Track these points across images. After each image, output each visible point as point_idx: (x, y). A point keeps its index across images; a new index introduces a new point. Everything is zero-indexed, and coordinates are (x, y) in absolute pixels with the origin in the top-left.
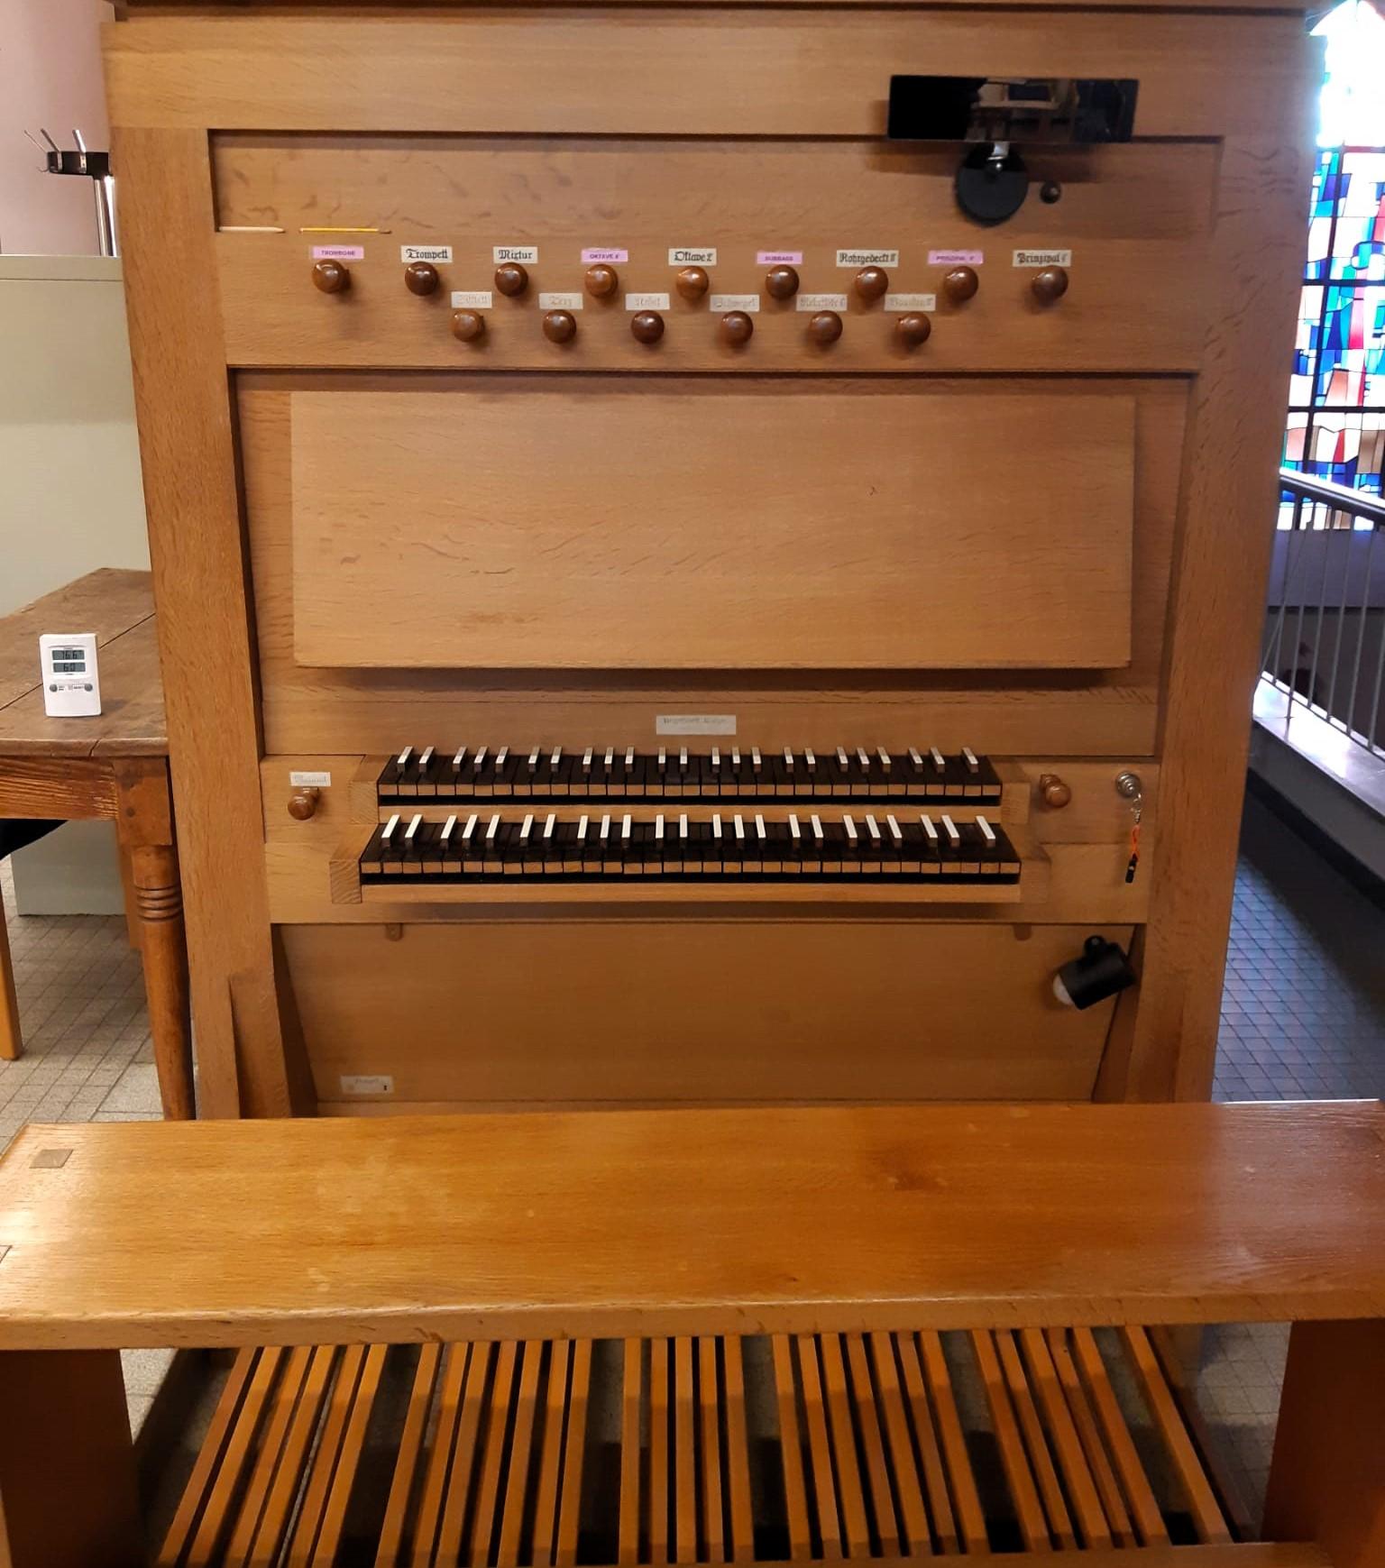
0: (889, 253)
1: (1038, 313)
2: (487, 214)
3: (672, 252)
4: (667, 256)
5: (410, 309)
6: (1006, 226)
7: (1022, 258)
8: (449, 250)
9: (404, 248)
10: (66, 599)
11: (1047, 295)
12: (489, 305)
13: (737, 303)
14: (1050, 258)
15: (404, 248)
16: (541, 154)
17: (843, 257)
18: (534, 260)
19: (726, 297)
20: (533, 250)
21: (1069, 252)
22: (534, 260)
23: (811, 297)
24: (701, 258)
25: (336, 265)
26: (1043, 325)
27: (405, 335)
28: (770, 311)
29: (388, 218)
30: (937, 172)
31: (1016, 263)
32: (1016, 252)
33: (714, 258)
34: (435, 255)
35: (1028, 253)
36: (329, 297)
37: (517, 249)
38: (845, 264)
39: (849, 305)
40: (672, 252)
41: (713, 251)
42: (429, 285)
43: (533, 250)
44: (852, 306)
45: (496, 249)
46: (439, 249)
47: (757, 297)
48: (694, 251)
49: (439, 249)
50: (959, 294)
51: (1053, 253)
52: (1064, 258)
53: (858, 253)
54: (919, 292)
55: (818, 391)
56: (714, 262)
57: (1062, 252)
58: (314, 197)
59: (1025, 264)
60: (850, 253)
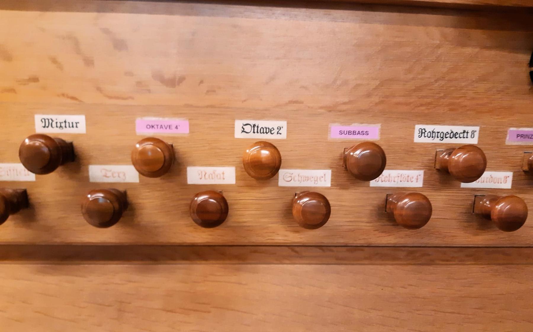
0: (470, 129)
2: (35, 79)
4: (289, 131)
7: (48, 124)
8: (283, 124)
13: (307, 179)
15: (477, 129)
16: (94, 14)
17: (422, 132)
18: (82, 129)
19: (296, 172)
20: (81, 119)
22: (82, 129)
24: (270, 131)
28: (343, 187)
30: (514, 49)
33: (284, 131)
36: (157, 180)
37: (61, 118)
38: (424, 140)
39: (425, 181)
40: (238, 124)
41: (283, 124)
43: (81, 119)
44: (336, 183)
48: (262, 124)
51: (458, 129)
54: (408, 168)
56: (284, 134)
60: (429, 128)
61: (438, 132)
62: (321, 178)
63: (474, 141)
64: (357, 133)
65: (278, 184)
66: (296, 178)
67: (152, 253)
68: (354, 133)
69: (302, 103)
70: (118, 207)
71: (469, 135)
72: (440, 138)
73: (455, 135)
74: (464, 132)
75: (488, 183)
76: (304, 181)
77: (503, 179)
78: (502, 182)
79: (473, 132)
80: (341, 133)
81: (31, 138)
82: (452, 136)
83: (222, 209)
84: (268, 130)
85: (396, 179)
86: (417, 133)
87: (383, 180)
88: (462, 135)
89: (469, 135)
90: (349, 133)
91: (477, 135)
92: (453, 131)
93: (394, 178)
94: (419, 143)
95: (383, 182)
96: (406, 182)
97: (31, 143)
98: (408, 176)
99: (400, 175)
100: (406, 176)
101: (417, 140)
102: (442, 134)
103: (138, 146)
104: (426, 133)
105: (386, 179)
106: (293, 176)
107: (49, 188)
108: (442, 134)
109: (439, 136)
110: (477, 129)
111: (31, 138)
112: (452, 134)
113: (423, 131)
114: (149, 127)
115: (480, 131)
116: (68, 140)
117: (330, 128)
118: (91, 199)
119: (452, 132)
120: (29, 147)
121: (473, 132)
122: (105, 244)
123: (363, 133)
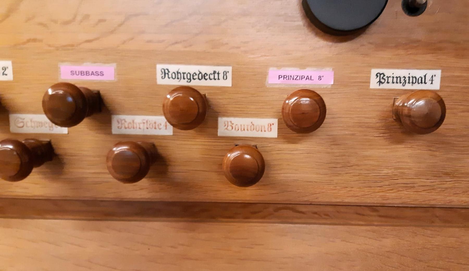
0: (221, 69)
1: (399, 142)
6: (362, 40)
7: (381, 78)
11: (415, 124)
12: (274, 133)
13: (253, 127)
14: (415, 80)
15: (229, 69)
17: (165, 73)
21: (438, 73)
23: (128, 118)
26: (408, 156)
31: (374, 84)
32: (374, 71)
33: (10, 72)
35: (388, 72)
47: (275, 121)
50: (306, 119)
51: (419, 73)
52: (433, 79)
53: (183, 68)
55: (327, 202)
57: (430, 73)
59: (385, 86)
60: (173, 68)
61: (184, 73)
62: (265, 127)
63: (436, 86)
64: (90, 73)
65: (217, 135)
66: (29, 124)
67: (194, 211)
68: (87, 73)
69: (41, 41)
70: (146, 160)
71: (221, 76)
72: (186, 80)
73: (204, 76)
74: (215, 72)
75: (267, 132)
76: (37, 127)
77: (266, 127)
78: (266, 130)
79: (225, 73)
80: (73, 73)
81: (55, 87)
82: (200, 77)
83: (175, 162)
84: (414, 79)
85: (142, 126)
86: (159, 75)
87: (127, 126)
88: (212, 77)
89: (221, 76)
90: (82, 73)
91: (229, 75)
92: (201, 71)
93: (139, 124)
94: (163, 85)
95: (128, 129)
96: (153, 129)
97: (54, 93)
98: (155, 123)
99: (145, 121)
100: (153, 122)
101: (160, 81)
102: (189, 75)
103: (168, 96)
104: (170, 74)
105: (130, 126)
106: (25, 121)
107: (80, 140)
108: (189, 75)
109: (185, 77)
110: (229, 69)
111: (55, 87)
112: (200, 75)
113: (167, 72)
114: (171, 75)
115: (233, 71)
116: (94, 88)
117: (60, 68)
118: (116, 152)
119: (200, 73)
120: (52, 96)
121: (225, 73)
122: (131, 200)
123: (97, 74)
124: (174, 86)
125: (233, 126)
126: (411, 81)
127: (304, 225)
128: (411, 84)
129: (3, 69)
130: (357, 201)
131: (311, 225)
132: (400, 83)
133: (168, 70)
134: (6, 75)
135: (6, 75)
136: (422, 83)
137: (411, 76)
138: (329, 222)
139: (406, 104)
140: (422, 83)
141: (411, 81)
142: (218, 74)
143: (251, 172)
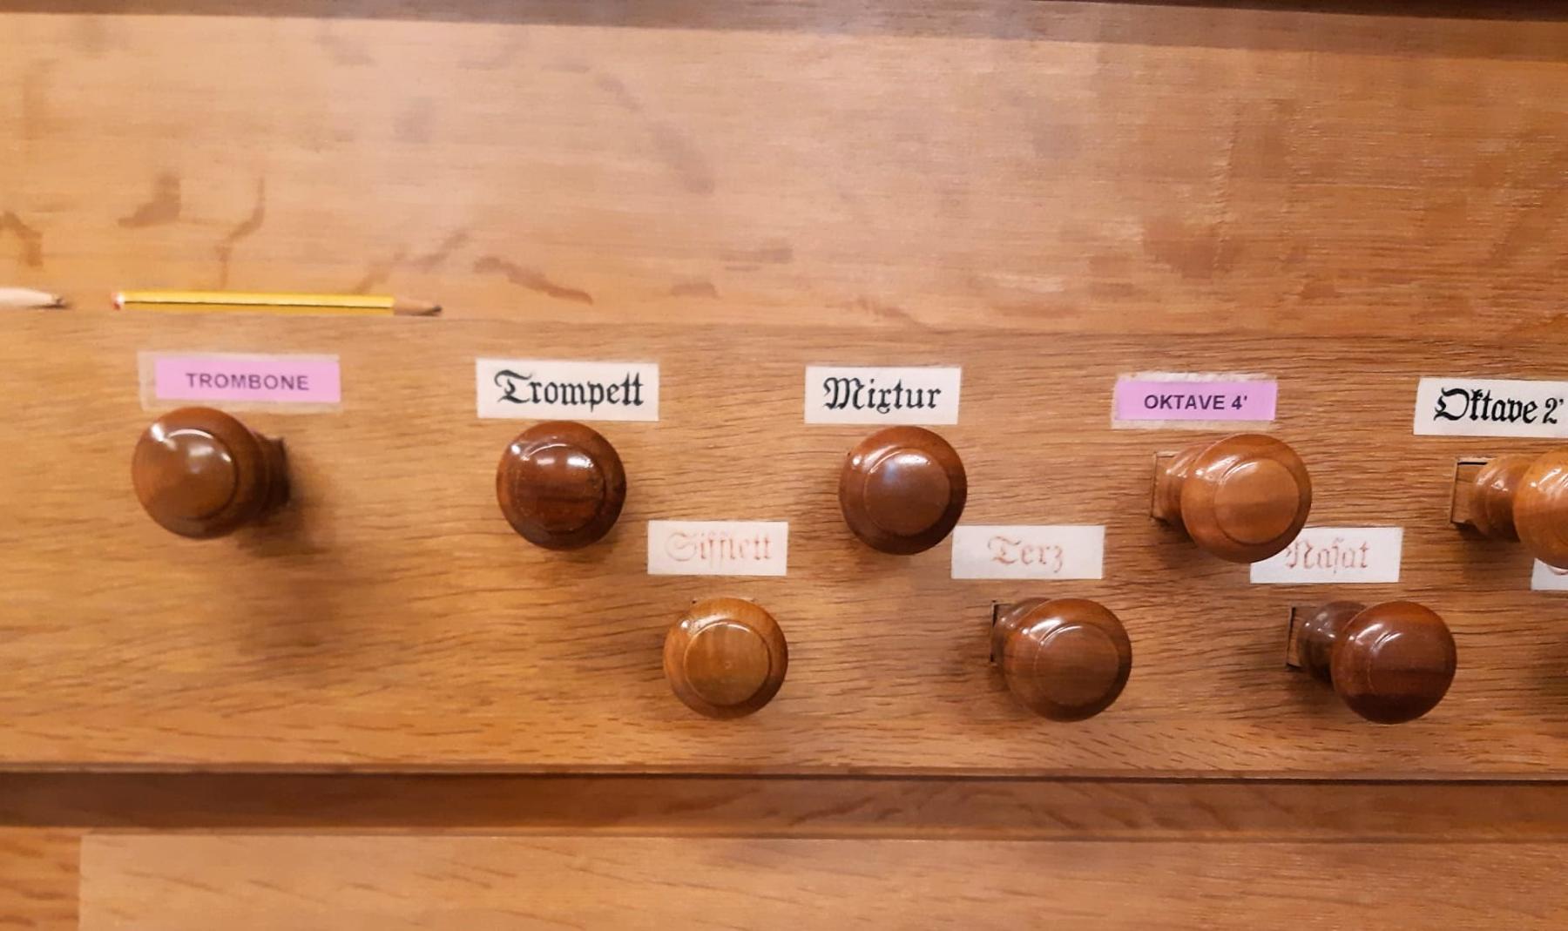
3: (1429, 390)
5: (503, 586)
7: (843, 395)
8: (650, 375)
9: (486, 368)
10: (1005, 688)
12: (776, 564)
20: (948, 379)
25: (229, 430)
27: (485, 659)
29: (432, 262)
34: (599, 394)
37: (886, 377)
40: (1429, 390)
42: (575, 506)
43: (948, 379)
45: (816, 376)
46: (610, 373)
48: (1501, 389)
49: (610, 373)
52: (1256, 401)
58: (168, 182)
68: (253, 381)
84: (597, 391)
114: (513, 392)
124: (873, 427)
125: (672, 545)
126: (587, 396)
127: (1079, 844)
128: (588, 405)
129: (1548, 406)
130: (1302, 766)
131: (1389, 846)
132: (583, 401)
133: (857, 380)
134: (1554, 422)
135: (1554, 422)
136: (1485, 417)
137: (877, 386)
138: (753, 831)
139: (1199, 473)
140: (920, 404)
141: (587, 396)
142: (1487, 399)
143: (743, 685)
